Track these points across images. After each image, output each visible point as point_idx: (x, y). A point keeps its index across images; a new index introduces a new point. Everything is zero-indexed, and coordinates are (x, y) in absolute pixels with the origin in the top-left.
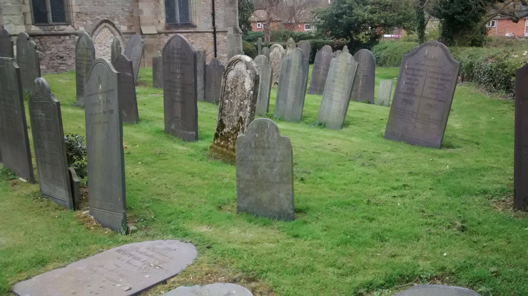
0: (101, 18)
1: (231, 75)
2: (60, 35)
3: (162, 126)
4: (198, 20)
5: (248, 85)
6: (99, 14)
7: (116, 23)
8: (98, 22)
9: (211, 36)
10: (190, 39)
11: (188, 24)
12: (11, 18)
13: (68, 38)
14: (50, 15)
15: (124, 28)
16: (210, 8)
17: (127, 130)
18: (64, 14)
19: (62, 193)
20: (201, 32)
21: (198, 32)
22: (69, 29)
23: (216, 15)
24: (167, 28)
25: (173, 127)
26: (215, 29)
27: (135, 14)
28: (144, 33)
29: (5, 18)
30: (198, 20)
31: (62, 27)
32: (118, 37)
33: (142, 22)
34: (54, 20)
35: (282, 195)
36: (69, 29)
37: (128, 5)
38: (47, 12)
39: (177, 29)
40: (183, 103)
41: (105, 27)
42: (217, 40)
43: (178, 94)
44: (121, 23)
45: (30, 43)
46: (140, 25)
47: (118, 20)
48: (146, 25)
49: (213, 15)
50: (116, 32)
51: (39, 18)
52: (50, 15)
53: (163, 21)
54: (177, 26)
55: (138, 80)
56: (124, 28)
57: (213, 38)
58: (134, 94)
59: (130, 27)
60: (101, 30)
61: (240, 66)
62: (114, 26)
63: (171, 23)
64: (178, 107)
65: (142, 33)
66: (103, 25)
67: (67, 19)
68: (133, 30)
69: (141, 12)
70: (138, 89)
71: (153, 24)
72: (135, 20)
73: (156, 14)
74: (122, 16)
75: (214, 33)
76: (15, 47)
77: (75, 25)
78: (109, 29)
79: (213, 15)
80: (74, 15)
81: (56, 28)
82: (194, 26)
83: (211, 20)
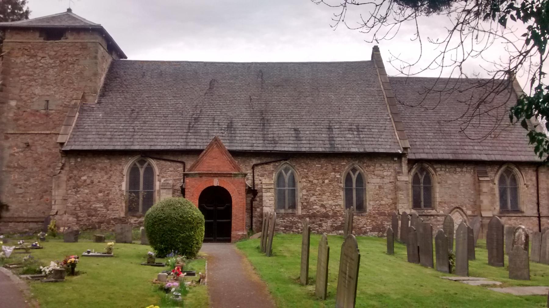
0: (454, 205)
1: (517, 234)
2: (428, 216)
3: (487, 262)
4: (525, 208)
5: (523, 238)
6: (453, 203)
7: (464, 209)
8: (452, 208)
9: (536, 219)
10: (518, 221)
11: (516, 210)
12: (403, 205)
13: (432, 217)
14: (422, 204)
15: (469, 213)
16: (535, 199)
17: (470, 262)
18: (431, 203)
19: (446, 269)
20: (528, 216)
21: (525, 216)
22: (433, 212)
23: (541, 204)
24: (501, 213)
25: (492, 261)
26: (539, 214)
27: (478, 203)
28: (256, 168)
29: (400, 205)
30: (525, 208)
31: (430, 211)
32: (465, 218)
33: (482, 208)
34: (425, 206)
35: (525, 273)
36: (433, 212)
37: (473, 197)
38: (421, 202)
39: (509, 213)
40: (497, 249)
41: (457, 211)
42: (541, 223)
43: (495, 244)
44: (467, 209)
45: (420, 219)
46: (480, 210)
47: (466, 207)
48: (485, 210)
49: (538, 204)
50: (464, 215)
51: (416, 204)
52: (422, 204)
53: (498, 208)
54: (508, 212)
55: (477, 245)
56: (469, 213)
57: (538, 221)
58: (474, 251)
59: (473, 212)
60: (454, 213)
61: (521, 230)
62: (462, 210)
63: (504, 210)
64: (495, 251)
65: (481, 216)
66: (456, 210)
67: (433, 206)
68: (476, 214)
69: (482, 202)
70: (476, 249)
71: (490, 210)
72: (477, 207)
73: (492, 203)
74: (469, 204)
75: (539, 217)
76: (410, 222)
77: (438, 210)
78: (460, 213)
79: (538, 204)
80: (437, 203)
81: (425, 211)
82: (522, 212)
83: (536, 207)
